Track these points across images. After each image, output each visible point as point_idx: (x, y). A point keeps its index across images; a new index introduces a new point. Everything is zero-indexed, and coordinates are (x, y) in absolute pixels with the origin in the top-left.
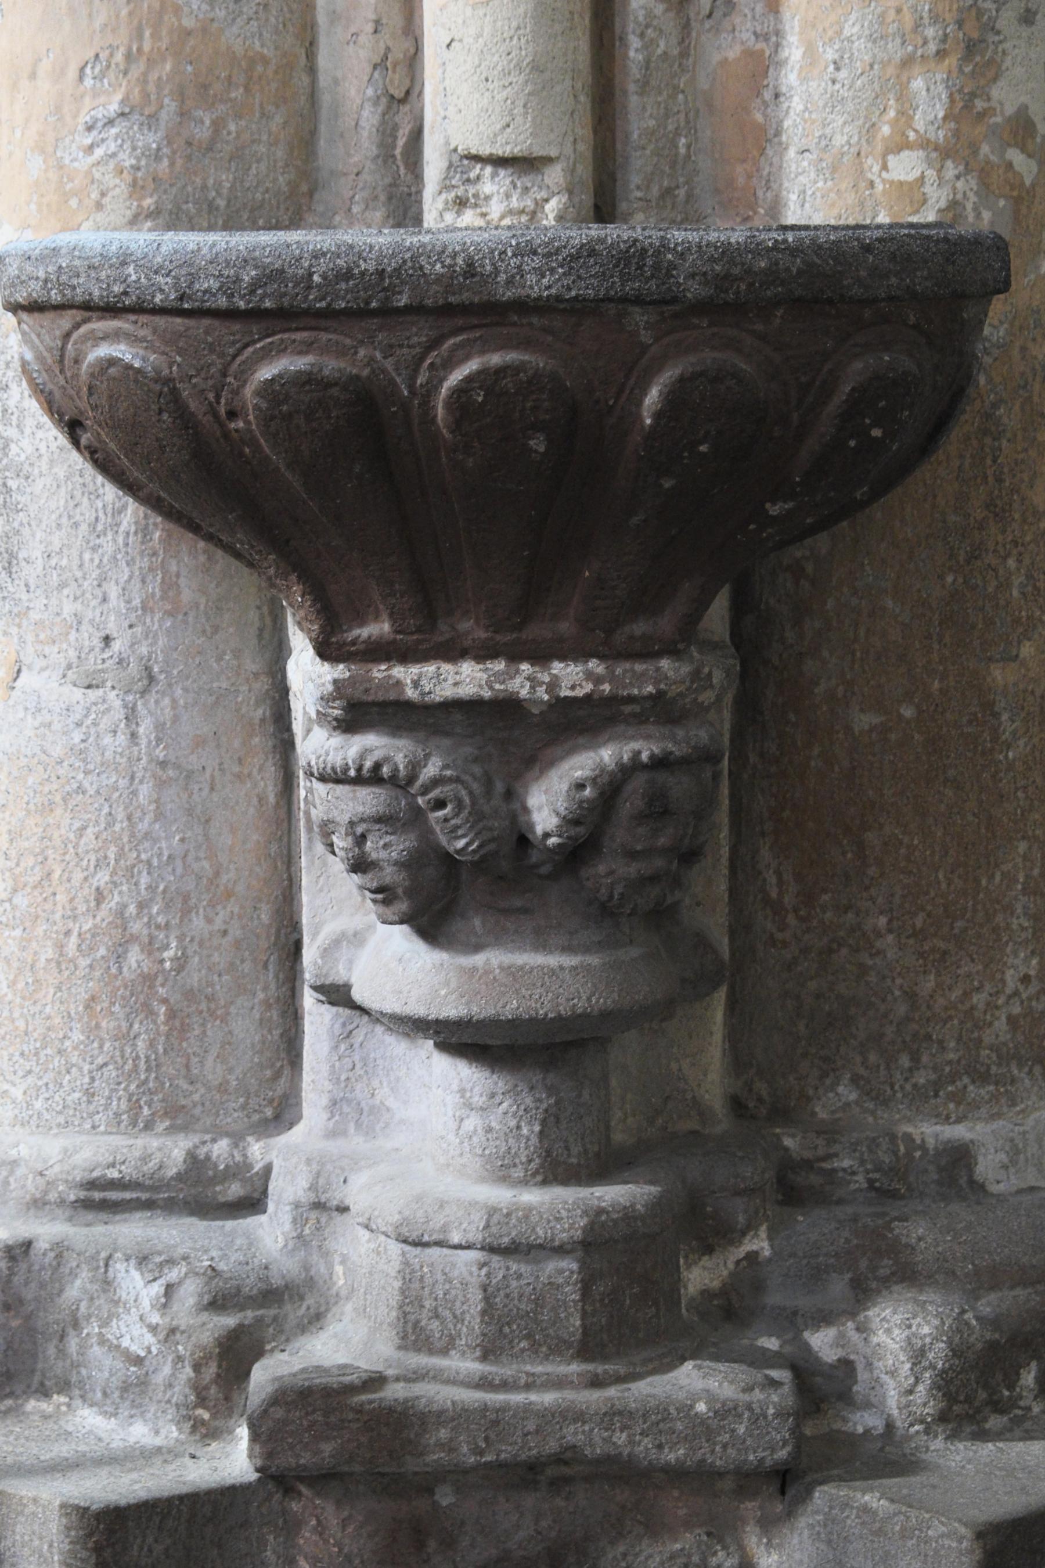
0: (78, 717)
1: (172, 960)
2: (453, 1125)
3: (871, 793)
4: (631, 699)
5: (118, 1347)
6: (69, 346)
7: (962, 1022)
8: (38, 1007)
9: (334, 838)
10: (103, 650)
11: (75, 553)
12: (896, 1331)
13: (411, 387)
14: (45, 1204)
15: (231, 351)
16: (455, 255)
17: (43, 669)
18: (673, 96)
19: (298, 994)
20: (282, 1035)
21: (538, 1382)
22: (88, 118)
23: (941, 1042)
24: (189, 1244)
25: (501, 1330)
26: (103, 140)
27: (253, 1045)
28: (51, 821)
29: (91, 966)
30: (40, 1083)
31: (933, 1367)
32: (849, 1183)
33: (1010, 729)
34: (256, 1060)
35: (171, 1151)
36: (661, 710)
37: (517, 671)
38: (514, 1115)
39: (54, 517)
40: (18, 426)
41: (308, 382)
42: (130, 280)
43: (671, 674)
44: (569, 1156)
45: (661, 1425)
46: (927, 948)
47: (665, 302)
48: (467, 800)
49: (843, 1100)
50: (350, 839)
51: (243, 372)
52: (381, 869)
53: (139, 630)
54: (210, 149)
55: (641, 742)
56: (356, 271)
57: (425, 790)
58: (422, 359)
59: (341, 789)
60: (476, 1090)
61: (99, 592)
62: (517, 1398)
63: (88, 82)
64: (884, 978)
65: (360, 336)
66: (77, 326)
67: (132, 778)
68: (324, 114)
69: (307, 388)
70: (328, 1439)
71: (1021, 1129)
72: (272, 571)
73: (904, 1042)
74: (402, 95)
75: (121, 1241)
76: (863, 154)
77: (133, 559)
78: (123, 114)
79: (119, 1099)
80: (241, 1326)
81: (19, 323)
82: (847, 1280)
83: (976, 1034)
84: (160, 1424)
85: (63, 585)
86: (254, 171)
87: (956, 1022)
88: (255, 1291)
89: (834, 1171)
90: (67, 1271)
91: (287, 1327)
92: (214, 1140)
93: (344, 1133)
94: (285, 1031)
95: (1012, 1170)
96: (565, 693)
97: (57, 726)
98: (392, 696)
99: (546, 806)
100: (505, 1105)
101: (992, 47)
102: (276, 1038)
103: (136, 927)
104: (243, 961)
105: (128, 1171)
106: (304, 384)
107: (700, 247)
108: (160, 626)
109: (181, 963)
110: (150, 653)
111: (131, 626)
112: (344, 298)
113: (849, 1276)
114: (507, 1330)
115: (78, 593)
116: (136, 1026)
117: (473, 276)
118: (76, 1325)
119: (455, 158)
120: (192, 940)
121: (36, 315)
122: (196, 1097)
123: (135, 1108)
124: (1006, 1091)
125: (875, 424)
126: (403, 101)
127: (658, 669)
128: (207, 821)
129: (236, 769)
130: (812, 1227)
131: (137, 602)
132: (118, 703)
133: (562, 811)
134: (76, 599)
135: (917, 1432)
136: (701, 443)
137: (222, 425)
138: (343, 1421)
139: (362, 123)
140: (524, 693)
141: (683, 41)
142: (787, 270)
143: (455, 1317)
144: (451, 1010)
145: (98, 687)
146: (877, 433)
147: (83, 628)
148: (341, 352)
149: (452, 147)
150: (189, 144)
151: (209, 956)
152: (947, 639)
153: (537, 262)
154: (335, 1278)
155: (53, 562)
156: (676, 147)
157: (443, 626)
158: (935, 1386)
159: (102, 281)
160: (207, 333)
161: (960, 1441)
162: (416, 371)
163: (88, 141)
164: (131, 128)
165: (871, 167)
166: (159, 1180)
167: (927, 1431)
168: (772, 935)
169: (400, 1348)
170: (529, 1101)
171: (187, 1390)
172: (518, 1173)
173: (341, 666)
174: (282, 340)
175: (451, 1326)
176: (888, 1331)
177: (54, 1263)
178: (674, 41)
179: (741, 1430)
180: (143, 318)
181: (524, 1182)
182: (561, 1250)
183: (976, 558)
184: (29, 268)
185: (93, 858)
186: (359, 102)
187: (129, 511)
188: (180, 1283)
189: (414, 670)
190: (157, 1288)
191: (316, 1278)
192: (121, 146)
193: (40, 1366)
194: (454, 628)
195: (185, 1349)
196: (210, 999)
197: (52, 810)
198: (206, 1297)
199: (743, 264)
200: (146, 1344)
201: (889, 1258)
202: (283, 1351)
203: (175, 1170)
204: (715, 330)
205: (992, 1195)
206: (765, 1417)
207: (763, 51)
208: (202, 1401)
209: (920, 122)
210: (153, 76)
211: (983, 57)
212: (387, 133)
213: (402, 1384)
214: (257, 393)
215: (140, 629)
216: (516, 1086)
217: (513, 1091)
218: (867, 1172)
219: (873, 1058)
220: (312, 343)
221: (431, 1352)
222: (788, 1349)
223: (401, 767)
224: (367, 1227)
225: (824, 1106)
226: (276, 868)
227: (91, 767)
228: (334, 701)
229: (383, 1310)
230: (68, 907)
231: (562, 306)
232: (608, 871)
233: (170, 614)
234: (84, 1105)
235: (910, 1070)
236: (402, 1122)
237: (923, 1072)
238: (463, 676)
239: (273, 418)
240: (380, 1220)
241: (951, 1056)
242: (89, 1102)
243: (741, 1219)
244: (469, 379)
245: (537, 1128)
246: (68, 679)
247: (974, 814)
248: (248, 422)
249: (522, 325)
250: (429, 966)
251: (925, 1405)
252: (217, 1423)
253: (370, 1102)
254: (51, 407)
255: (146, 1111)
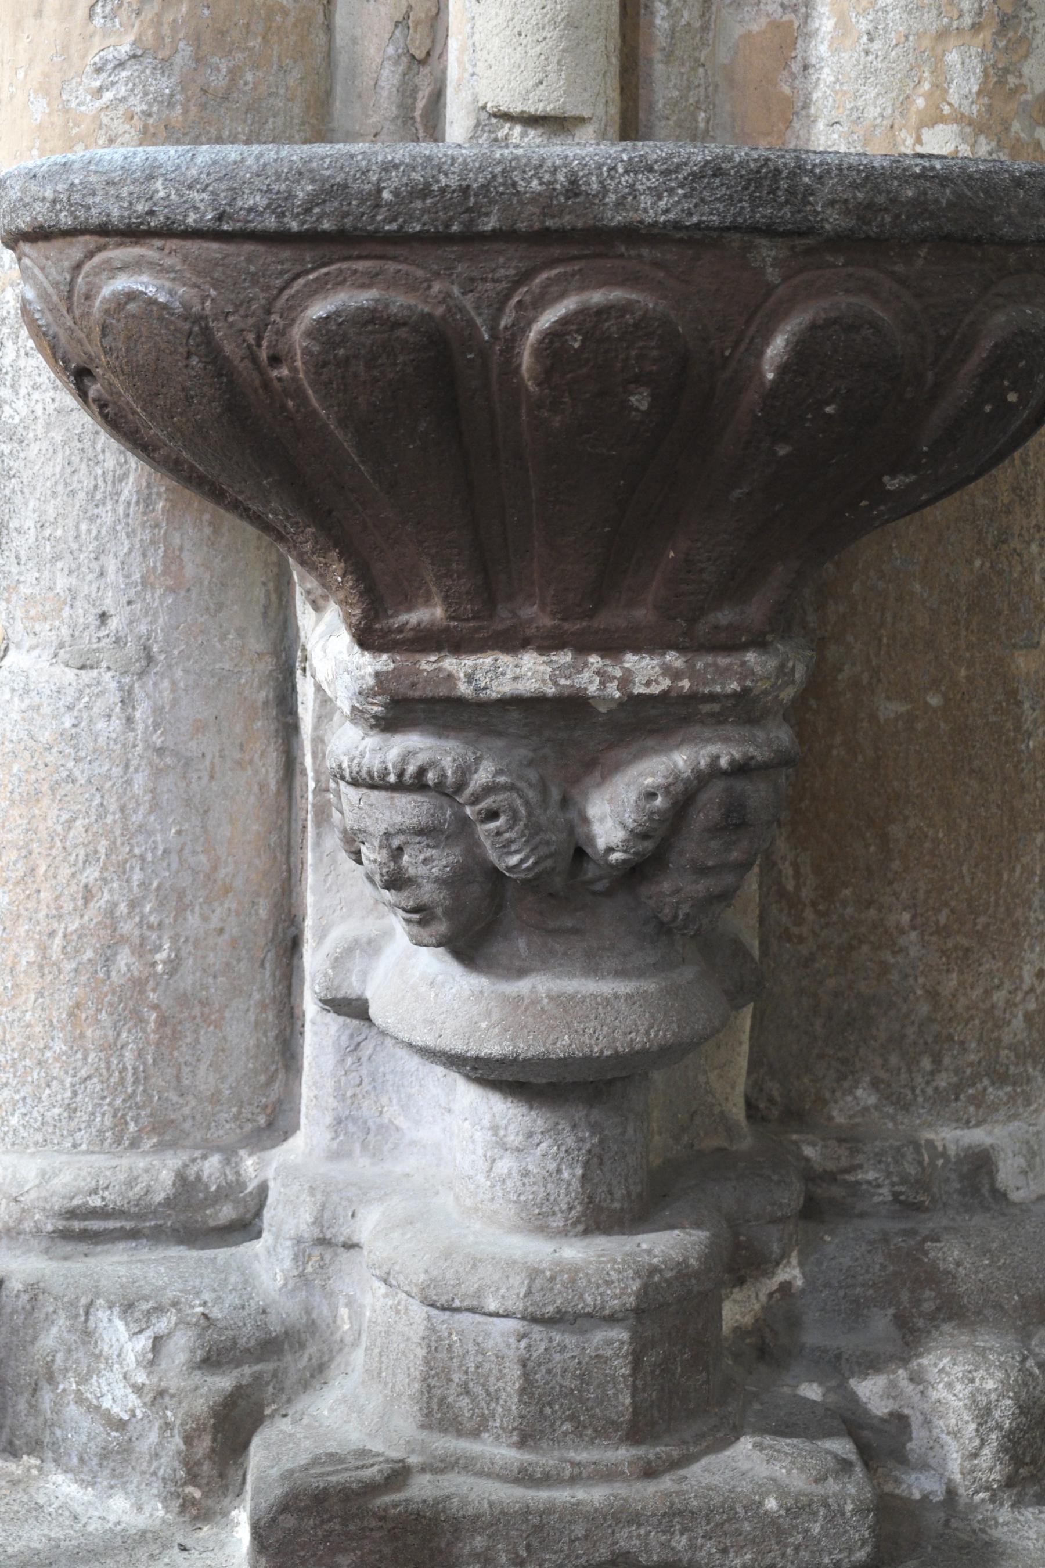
0: (69, 699)
1: (164, 963)
2: (483, 1166)
3: (896, 783)
4: (712, 697)
5: (98, 1408)
6: (80, 279)
7: (983, 1022)
8: (18, 1014)
9: (364, 849)
10: (99, 628)
11: (70, 522)
12: (959, 1387)
13: (493, 329)
14: (19, 1234)
15: (278, 283)
16: (555, 170)
17: (32, 648)
18: (693, 69)
19: (294, 993)
20: (276, 1038)
21: (585, 1475)
22: (97, 59)
23: (962, 1043)
24: (179, 1285)
25: (541, 1411)
26: (113, 84)
27: (247, 1050)
28: (37, 812)
29: (76, 970)
30: (17, 1097)
31: (999, 1427)
32: (873, 1195)
33: (1030, 718)
34: (251, 1066)
35: (157, 1172)
36: (743, 709)
37: (586, 665)
38: (554, 1158)
39: (48, 484)
40: (12, 386)
41: (372, 321)
42: (157, 196)
43: (757, 669)
44: (612, 1200)
45: (726, 1526)
46: (950, 945)
47: (800, 234)
48: (523, 811)
49: (862, 1103)
50: (384, 851)
51: (291, 308)
52: (419, 886)
53: (138, 606)
54: (225, 99)
55: (719, 745)
56: (435, 187)
57: (475, 800)
58: (508, 297)
59: (375, 795)
60: (512, 1128)
61: (95, 565)
62: (563, 1495)
63: (98, 21)
64: (906, 976)
65: (435, 267)
66: (90, 255)
67: (127, 766)
68: (341, 74)
69: (370, 328)
70: (344, 1551)
71: (1035, 1129)
72: (309, 546)
73: (926, 1043)
74: (423, 56)
75: (104, 1282)
76: (896, 126)
77: (134, 531)
78: (134, 56)
79: (104, 1115)
80: (238, 1388)
81: (19, 259)
82: (890, 1317)
83: (996, 1034)
84: (144, 1498)
85: (56, 558)
86: (270, 125)
87: (977, 1022)
88: (253, 1342)
89: (858, 1183)
90: (42, 1316)
91: (288, 1383)
92: (204, 1157)
93: (348, 1155)
94: (280, 1031)
95: (1031, 1175)
96: (639, 689)
97: (46, 710)
98: (442, 692)
99: (611, 816)
100: (544, 1145)
101: (1024, 23)
102: (271, 1039)
103: (127, 927)
104: (239, 960)
105: (112, 1198)
106: (366, 323)
107: (841, 170)
108: (161, 603)
109: (174, 966)
110: (149, 632)
111: (129, 603)
112: (419, 220)
113: (891, 1311)
114: (548, 1411)
115: (74, 566)
116: (124, 1035)
117: (577, 195)
118: (51, 1379)
119: (484, 116)
120: (187, 940)
121: (41, 244)
122: (186, 1111)
123: (120, 1123)
124: (1023, 1091)
125: (1013, 388)
126: (422, 62)
127: (743, 664)
128: (206, 812)
129: (238, 756)
130: (844, 1248)
131: (137, 577)
132: (113, 685)
133: (631, 825)
134: (70, 572)
135: (983, 1500)
136: (828, 404)
137: (262, 373)
138: (363, 1529)
139: (381, 83)
140: (593, 689)
141: (703, 15)
142: (937, 201)
143: (488, 1394)
144: (494, 1048)
145: (92, 667)
146: (1012, 397)
147: (78, 604)
148: (411, 287)
149: (480, 104)
150: (205, 92)
151: (204, 957)
152: (974, 626)
153: (653, 180)
154: (339, 1322)
155: (47, 532)
156: (697, 122)
157: (502, 611)
158: (1003, 1449)
159: (123, 198)
160: (249, 260)
161: (1026, 1507)
162: (500, 310)
163: (98, 84)
164: (143, 72)
165: (904, 141)
166: (148, 1206)
167: (993, 1500)
168: (787, 929)
169: (423, 1427)
170: (570, 1141)
171: (176, 1464)
172: (557, 1222)
173: (385, 657)
174: (341, 271)
175: (483, 1404)
176: (950, 1386)
177: (28, 1307)
178: (696, 13)
179: (816, 1529)
180: (172, 244)
181: (564, 1233)
182: (612, 1319)
183: (1003, 542)
184: (34, 187)
185: (82, 853)
186: (379, 60)
187: (131, 479)
188: (169, 1335)
189: (469, 661)
190: (143, 1342)
191: (319, 1321)
192: (132, 90)
193: (8, 1422)
194: (515, 615)
195: (175, 1415)
196: (204, 1003)
197: (38, 800)
198: (199, 1352)
199: (889, 192)
200: (130, 1405)
201: (931, 1289)
202: (285, 1416)
203: (163, 1195)
204: (850, 270)
205: (1014, 1204)
206: (843, 1514)
207: (791, 22)
208: (193, 1478)
209: (954, 97)
210: (168, 18)
211: (1016, 32)
212: (407, 93)
213: (428, 1477)
214: (309, 334)
215: (139, 606)
216: (557, 1124)
217: (553, 1130)
218: (893, 1184)
219: (894, 1060)
220: (377, 274)
221: (460, 1433)
222: (832, 1398)
223: (449, 773)
224: (385, 1281)
225: (841, 1110)
226: (275, 858)
227: (82, 754)
228: (374, 696)
229: (402, 1380)
230: (53, 906)
231: (679, 235)
232: (674, 890)
233: (171, 590)
234: (64, 1122)
235: (932, 1073)
236: (413, 1143)
237: (944, 1075)
238: (524, 669)
239: (325, 364)
240: (401, 1277)
241: (972, 1057)
242: (70, 1118)
243: (776, 1248)
244: (565, 321)
245: (579, 1172)
246: (59, 659)
247: (998, 806)
248: (294, 370)
249: (630, 257)
250: (468, 993)
251: (991, 1470)
252: (209, 1502)
253: (378, 1120)
254: (54, 351)
255: (132, 1127)
